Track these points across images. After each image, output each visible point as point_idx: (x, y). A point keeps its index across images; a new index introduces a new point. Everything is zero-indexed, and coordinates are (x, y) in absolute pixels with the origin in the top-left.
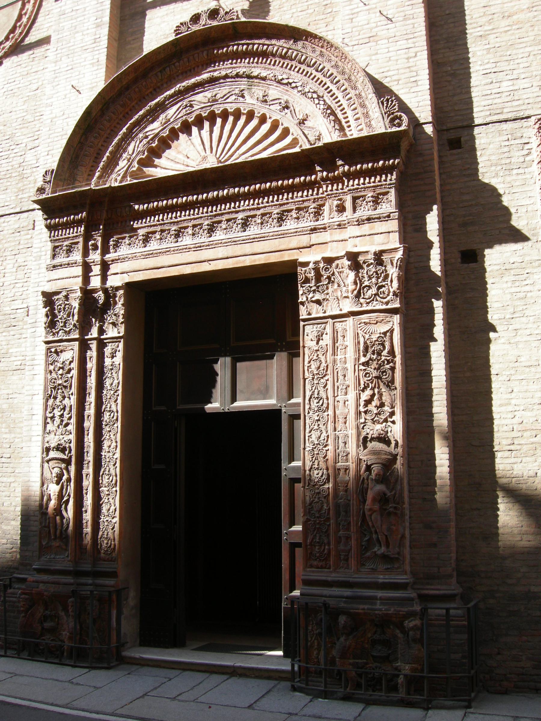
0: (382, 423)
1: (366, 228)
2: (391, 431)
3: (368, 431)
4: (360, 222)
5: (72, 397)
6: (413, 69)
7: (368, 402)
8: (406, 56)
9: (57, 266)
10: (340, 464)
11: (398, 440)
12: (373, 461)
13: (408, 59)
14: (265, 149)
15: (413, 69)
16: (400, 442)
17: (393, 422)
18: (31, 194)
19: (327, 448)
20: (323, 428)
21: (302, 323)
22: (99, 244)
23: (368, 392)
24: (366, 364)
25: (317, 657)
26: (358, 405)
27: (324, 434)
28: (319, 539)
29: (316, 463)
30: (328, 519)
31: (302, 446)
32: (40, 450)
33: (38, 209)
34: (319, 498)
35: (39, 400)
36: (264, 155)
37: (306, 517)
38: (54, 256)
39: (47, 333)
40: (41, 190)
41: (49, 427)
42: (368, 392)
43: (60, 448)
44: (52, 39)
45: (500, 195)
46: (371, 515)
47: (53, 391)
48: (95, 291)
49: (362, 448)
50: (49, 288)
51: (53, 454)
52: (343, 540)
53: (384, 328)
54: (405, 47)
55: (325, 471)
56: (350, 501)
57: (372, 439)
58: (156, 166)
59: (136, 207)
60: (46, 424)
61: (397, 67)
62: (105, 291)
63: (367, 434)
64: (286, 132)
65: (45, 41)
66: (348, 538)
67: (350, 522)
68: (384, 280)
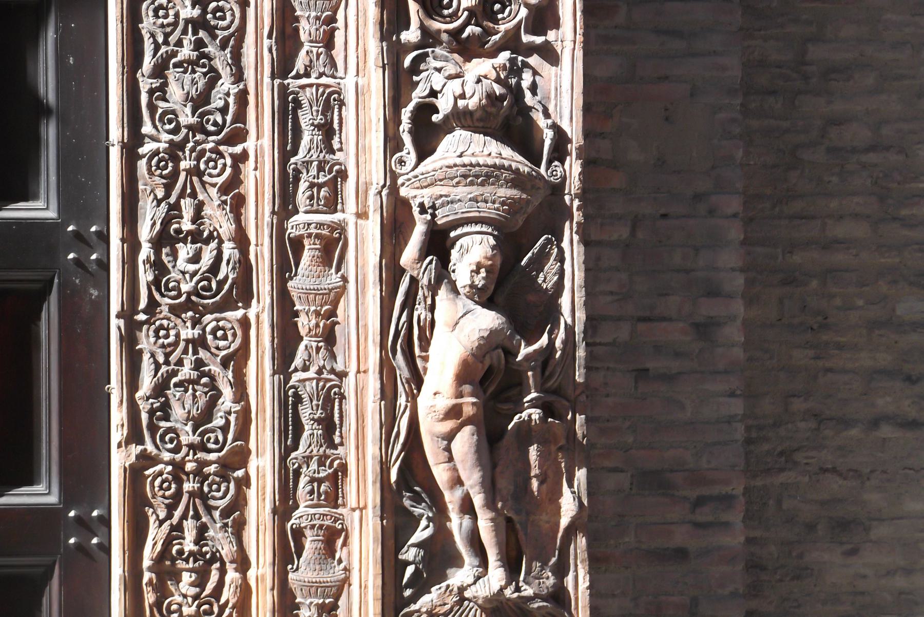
0: (493, 54)
2: (534, 88)
3: (437, 81)
10: (301, 218)
11: (565, 126)
12: (461, 210)
16: (574, 130)
17: (550, 55)
19: (238, 149)
20: (222, 61)
22: (528, 95)
25: (895, 219)
27: (226, 84)
28: (196, 543)
29: (187, 208)
30: (241, 457)
31: (116, 132)
34: (199, 364)
37: (135, 450)
46: (450, 437)
49: (409, 152)
52: (310, 544)
55: (229, 249)
56: (342, 375)
57: (462, 118)
63: (433, 93)
66: (332, 538)
67: (344, 468)
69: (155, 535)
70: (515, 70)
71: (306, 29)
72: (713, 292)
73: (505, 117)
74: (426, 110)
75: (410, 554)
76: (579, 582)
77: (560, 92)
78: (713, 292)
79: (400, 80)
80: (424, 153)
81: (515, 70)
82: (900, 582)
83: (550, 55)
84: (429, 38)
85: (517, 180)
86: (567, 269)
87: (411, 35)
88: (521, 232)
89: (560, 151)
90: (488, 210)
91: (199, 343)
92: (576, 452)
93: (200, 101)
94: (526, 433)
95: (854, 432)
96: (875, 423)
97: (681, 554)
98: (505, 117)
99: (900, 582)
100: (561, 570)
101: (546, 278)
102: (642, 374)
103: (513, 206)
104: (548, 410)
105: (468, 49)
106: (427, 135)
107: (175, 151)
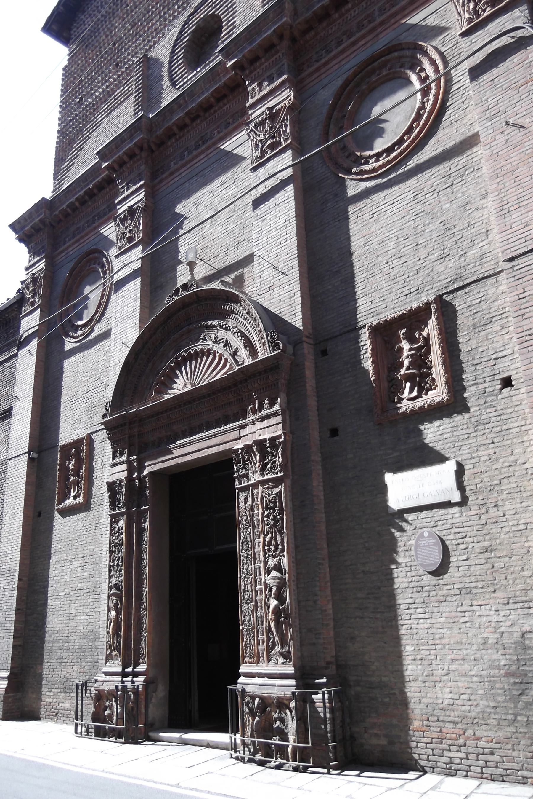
1: (266, 423)
4: (262, 419)
5: (123, 551)
6: (293, 305)
7: (269, 544)
8: (289, 297)
9: (269, 415)
13: (290, 298)
14: (217, 374)
15: (293, 305)
17: (284, 556)
18: (99, 419)
21: (237, 491)
23: (269, 536)
24: (267, 516)
26: (264, 546)
27: (250, 567)
32: (107, 587)
33: (102, 430)
35: (105, 556)
36: (218, 377)
38: (114, 458)
39: (111, 509)
40: (104, 416)
41: (113, 573)
42: (269, 536)
43: (116, 586)
44: (481, 136)
45: (461, 351)
47: (113, 548)
48: (135, 479)
50: (111, 479)
51: (114, 591)
53: (277, 490)
54: (288, 290)
58: (174, 389)
59: (403, 331)
60: (110, 571)
61: (284, 305)
62: (140, 480)
64: (226, 360)
65: (469, 143)
68: (275, 458)
69: (245, 640)
70: (280, 559)
71: (257, 556)
72: (316, 595)
73: (278, 568)
74: (269, 568)
75: (270, 644)
76: (292, 649)
77: (285, 562)
78: (316, 595)
79: (266, 563)
80: (268, 575)
81: (280, 559)
82: (362, 650)
83: (284, 556)
84: (269, 556)
85: (279, 578)
86: (287, 593)
87: (267, 556)
88: (281, 586)
89: (285, 574)
90: (276, 584)
91: (248, 609)
92: (291, 626)
93: (247, 569)
94: (283, 623)
95: (353, 620)
96: (356, 618)
97: (314, 644)
98: (278, 568)
99: (362, 650)
100: (289, 647)
101: (284, 595)
102: (307, 611)
103: (279, 583)
104: (285, 618)
105: (274, 557)
106: (269, 572)
107: (245, 577)
